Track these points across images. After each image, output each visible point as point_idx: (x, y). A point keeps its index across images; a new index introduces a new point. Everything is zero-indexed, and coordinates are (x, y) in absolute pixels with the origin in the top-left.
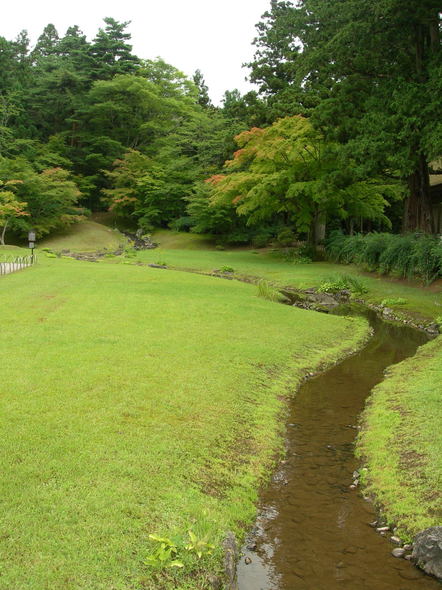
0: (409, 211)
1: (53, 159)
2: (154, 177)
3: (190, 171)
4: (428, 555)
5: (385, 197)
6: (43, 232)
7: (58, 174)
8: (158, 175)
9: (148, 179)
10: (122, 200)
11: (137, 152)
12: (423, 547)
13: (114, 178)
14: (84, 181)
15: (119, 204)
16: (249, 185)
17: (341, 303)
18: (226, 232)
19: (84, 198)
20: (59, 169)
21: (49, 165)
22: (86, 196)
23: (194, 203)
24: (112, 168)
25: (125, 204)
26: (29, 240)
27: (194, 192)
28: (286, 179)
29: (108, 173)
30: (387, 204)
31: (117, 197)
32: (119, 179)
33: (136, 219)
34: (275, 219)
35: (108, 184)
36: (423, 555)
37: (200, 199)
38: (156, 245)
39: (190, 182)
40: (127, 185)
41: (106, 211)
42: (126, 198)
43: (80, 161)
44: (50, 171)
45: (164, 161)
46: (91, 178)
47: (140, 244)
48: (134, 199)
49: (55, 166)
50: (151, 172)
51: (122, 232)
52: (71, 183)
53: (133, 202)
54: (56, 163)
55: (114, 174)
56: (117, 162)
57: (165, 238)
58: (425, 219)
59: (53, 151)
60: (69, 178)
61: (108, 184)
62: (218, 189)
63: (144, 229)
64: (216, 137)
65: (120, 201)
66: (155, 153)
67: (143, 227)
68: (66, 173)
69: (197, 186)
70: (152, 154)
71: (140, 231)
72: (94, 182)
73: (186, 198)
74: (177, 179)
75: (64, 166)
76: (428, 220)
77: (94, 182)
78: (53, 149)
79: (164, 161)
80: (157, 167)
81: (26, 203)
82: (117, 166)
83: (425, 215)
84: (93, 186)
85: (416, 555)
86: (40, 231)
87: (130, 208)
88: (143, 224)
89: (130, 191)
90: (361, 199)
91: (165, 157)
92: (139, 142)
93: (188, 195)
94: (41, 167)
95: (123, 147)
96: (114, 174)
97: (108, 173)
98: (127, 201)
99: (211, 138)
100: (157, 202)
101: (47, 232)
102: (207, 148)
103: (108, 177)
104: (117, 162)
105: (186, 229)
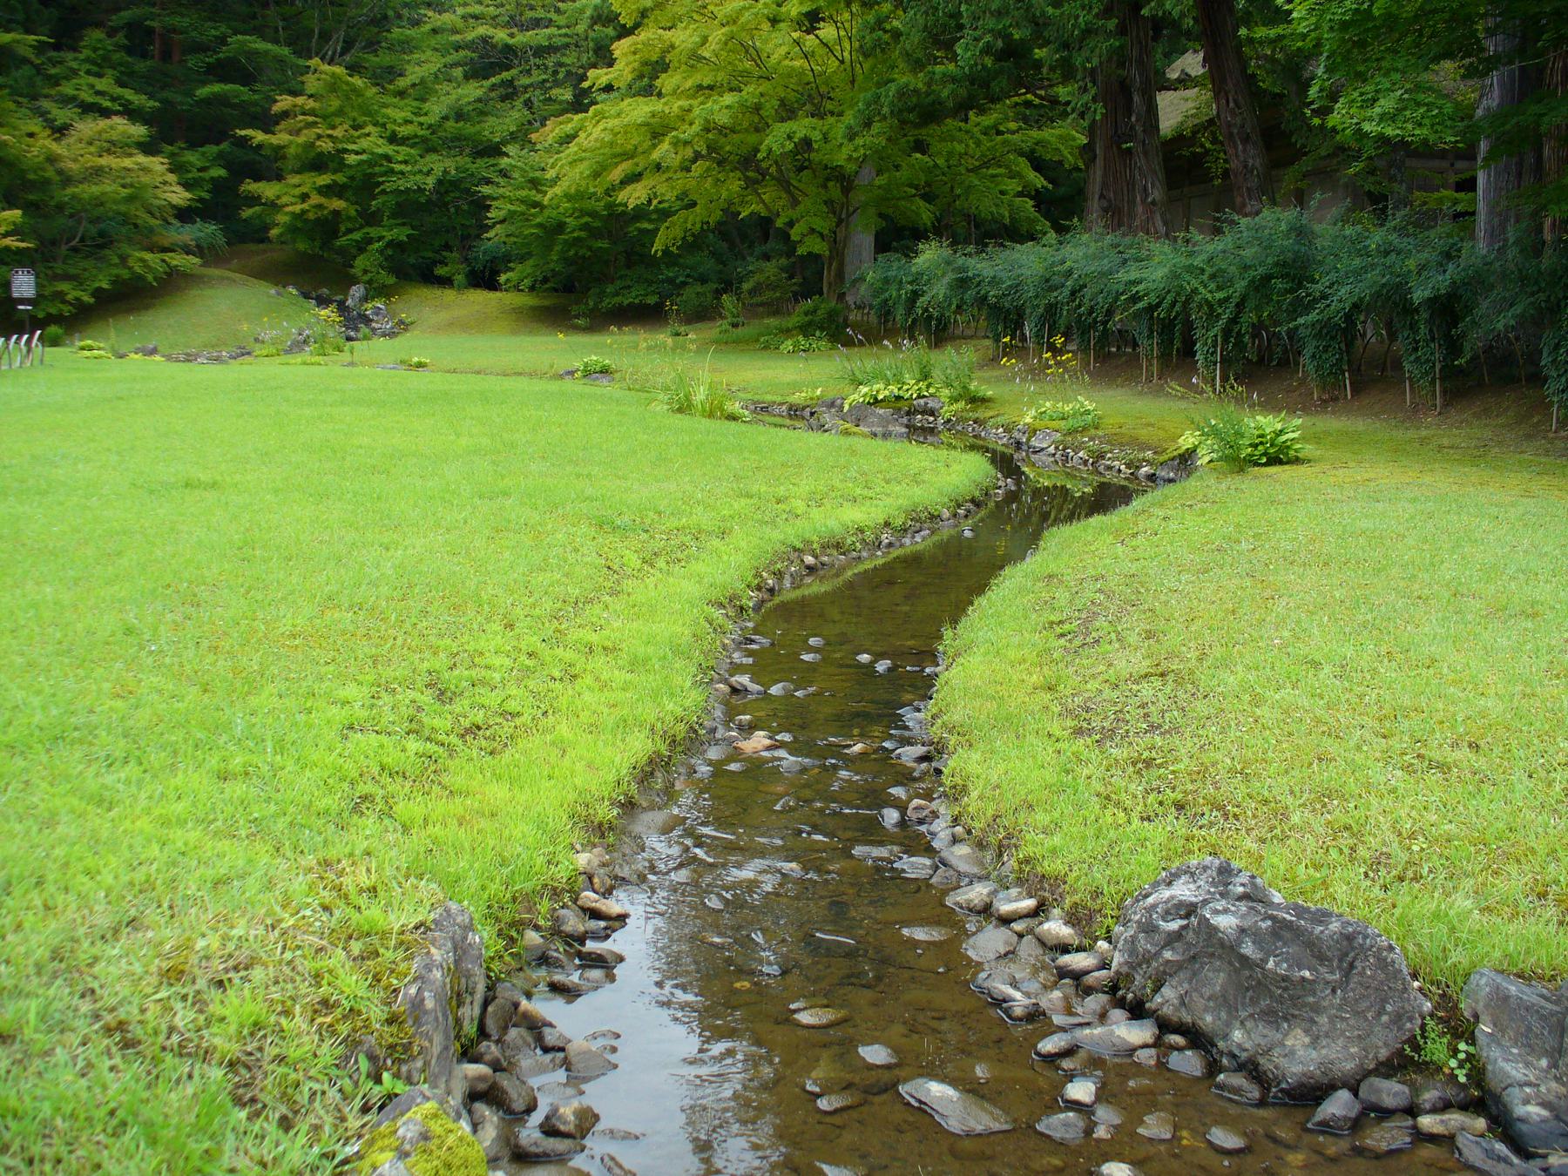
0: (1102, 196)
1: (98, 93)
2: (393, 139)
3: (491, 120)
4: (1168, 955)
5: (1038, 165)
6: (77, 299)
7: (114, 136)
8: (404, 131)
9: (373, 142)
10: (305, 206)
11: (339, 70)
12: (1149, 929)
13: (281, 147)
14: (192, 157)
15: (295, 216)
16: (656, 131)
17: (917, 423)
18: (602, 277)
19: (194, 204)
20: (117, 120)
21: (88, 109)
22: (201, 200)
23: (503, 201)
24: (268, 122)
25: (311, 216)
26: (15, 295)
27: (504, 174)
28: (757, 108)
29: (259, 137)
30: (1039, 181)
31: (288, 197)
32: (292, 151)
33: (348, 257)
34: (738, 237)
35: (268, 166)
36: (1147, 959)
37: (524, 193)
38: (403, 326)
39: (495, 150)
40: (318, 163)
41: (262, 241)
42: (316, 199)
43: (182, 103)
44: (89, 127)
45: (422, 91)
46: (212, 149)
47: (355, 323)
48: (338, 204)
49: (106, 113)
50: (384, 126)
51: (306, 296)
52: (157, 164)
53: (336, 213)
54: (107, 104)
55: (280, 138)
56: (284, 102)
57: (429, 308)
58: (1144, 201)
59: (95, 69)
60: (148, 148)
61: (268, 166)
62: (572, 158)
63: (370, 282)
64: (561, 20)
65: (298, 208)
66: (393, 72)
67: (366, 278)
68: (139, 131)
69: (513, 156)
70: (385, 76)
71: (357, 291)
72: (221, 159)
73: (486, 190)
74: (455, 143)
75: (131, 113)
76: (1153, 203)
77: (221, 159)
78: (94, 63)
79: (422, 91)
80: (397, 113)
81: (18, 212)
82: (285, 114)
83: (1145, 189)
84: (219, 172)
85: (1127, 963)
86: (69, 297)
87: (327, 227)
88: (365, 272)
89: (324, 179)
90: (969, 170)
91: (423, 81)
92: (348, 45)
93: (488, 182)
94: (61, 115)
95: (301, 62)
96: (280, 138)
97: (259, 137)
98: (320, 206)
99: (550, 23)
100: (409, 207)
101: (87, 299)
102: (540, 51)
103: (260, 146)
104: (284, 102)
105: (485, 279)
